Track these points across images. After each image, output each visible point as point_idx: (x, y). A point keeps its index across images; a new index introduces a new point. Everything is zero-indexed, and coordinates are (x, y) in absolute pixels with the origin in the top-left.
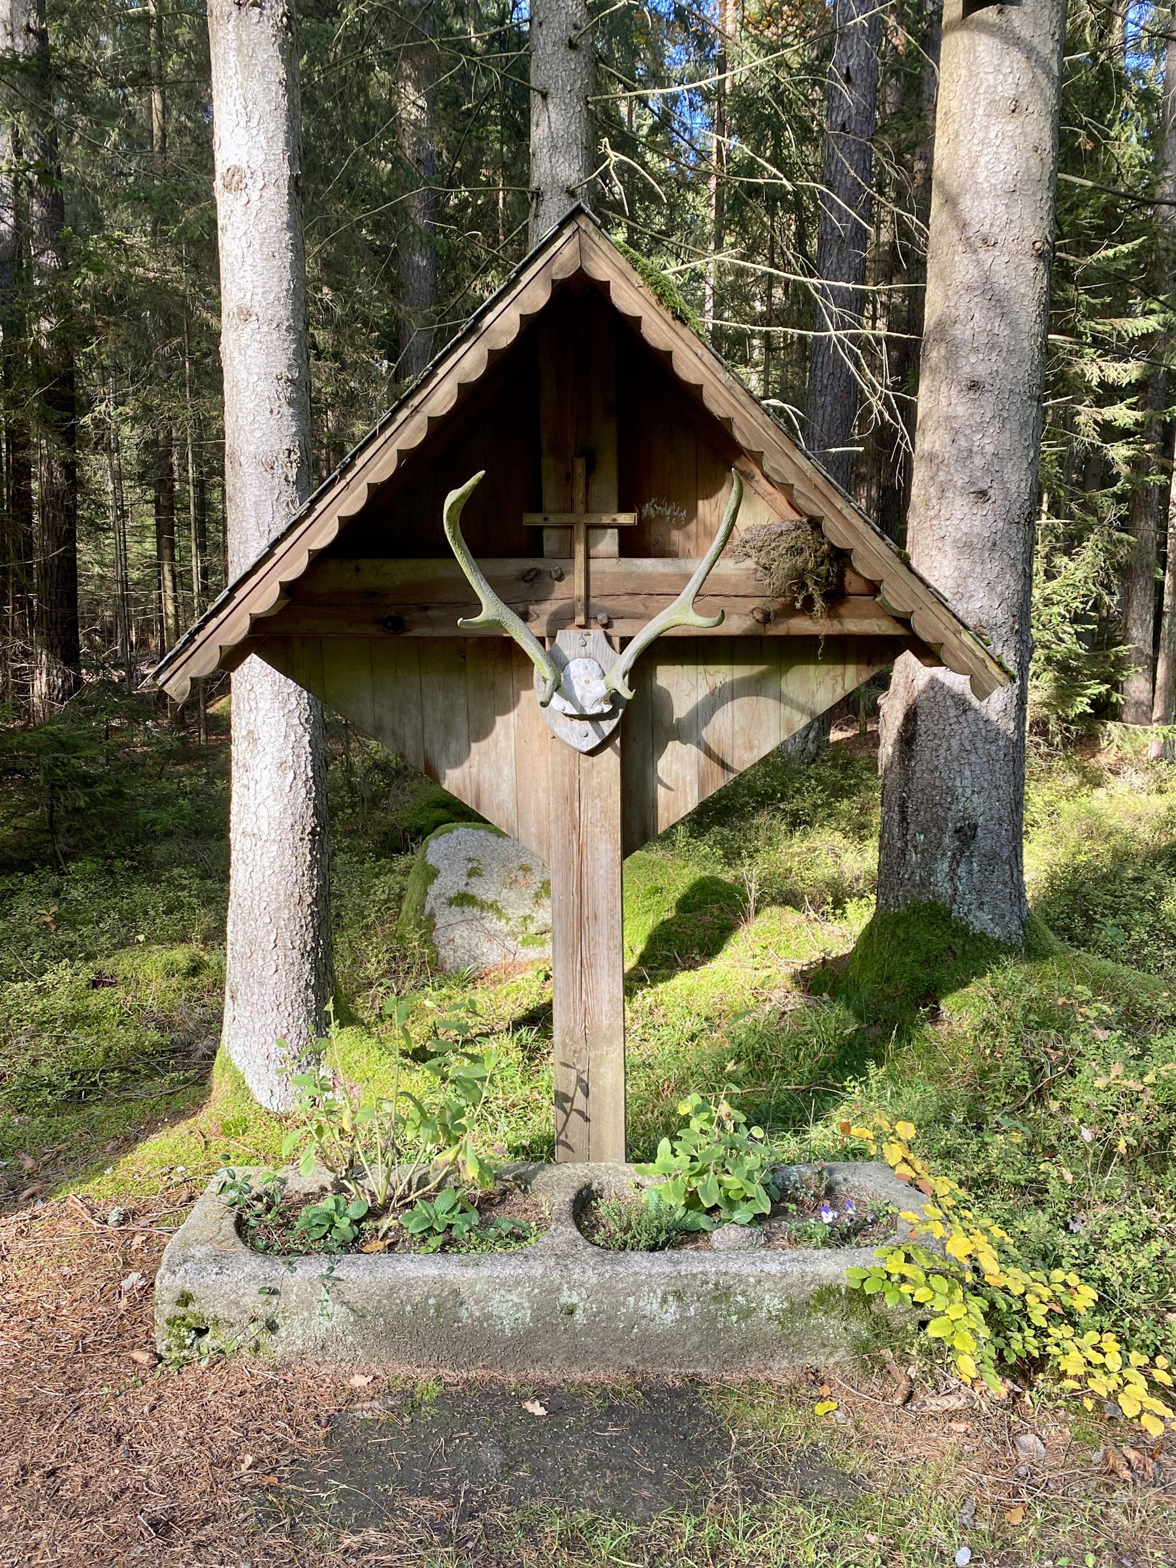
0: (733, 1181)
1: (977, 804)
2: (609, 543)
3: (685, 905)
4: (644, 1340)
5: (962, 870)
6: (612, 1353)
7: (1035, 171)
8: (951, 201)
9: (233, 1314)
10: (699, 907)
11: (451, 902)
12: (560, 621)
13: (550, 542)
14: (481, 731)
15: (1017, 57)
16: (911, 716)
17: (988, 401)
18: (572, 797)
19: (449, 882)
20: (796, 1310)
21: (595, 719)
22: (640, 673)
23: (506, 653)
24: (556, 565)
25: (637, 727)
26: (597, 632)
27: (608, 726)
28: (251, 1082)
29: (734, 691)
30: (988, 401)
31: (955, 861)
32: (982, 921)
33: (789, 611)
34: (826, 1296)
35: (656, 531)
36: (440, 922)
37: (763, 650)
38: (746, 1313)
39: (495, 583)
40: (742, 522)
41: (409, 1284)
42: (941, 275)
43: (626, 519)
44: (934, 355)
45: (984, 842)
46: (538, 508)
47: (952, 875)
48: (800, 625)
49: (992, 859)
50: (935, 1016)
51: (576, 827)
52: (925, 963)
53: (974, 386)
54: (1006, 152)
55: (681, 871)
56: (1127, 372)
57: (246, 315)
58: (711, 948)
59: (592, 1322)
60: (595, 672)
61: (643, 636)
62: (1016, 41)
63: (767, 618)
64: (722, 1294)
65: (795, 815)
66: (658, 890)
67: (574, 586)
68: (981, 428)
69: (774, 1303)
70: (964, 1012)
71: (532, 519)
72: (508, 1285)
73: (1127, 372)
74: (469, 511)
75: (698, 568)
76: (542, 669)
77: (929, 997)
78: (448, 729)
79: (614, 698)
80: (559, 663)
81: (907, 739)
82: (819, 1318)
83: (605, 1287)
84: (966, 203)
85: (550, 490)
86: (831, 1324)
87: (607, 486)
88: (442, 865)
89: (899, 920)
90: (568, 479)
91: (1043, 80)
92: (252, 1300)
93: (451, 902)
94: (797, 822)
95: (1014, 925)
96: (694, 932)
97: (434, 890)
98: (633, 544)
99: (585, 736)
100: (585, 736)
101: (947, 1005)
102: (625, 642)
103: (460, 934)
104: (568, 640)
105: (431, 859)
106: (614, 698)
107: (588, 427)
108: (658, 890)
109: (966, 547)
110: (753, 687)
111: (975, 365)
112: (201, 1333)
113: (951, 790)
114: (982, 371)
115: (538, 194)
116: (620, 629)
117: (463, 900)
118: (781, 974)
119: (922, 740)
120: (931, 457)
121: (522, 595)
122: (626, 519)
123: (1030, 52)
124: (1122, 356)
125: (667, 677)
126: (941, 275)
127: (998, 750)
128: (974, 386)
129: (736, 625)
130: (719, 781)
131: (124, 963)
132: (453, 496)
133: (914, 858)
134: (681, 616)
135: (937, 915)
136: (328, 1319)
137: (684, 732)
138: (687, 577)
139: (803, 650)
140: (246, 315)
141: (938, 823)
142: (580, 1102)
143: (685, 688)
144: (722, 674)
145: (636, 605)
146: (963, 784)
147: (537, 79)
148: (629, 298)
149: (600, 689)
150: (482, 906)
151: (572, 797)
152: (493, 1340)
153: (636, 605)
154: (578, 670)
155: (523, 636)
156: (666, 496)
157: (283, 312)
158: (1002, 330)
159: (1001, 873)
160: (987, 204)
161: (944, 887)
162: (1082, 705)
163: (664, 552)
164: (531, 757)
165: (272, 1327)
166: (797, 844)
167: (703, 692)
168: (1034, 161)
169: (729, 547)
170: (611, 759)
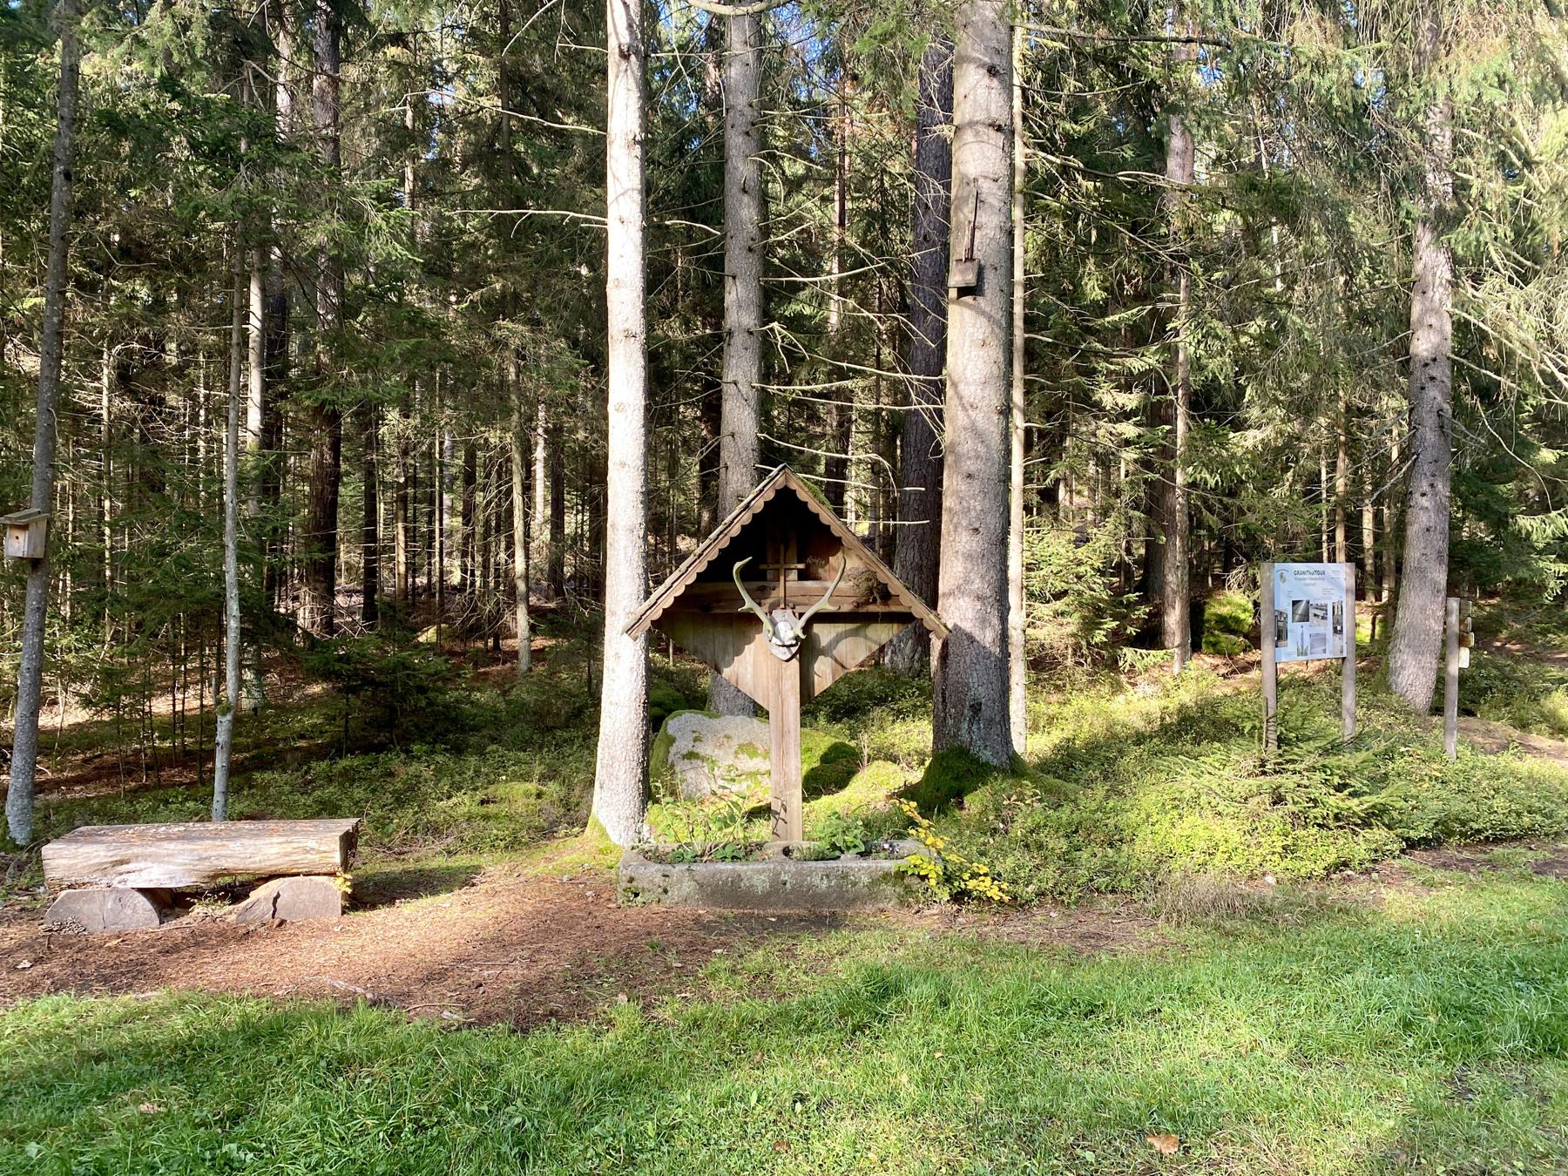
0: (849, 839)
1: (981, 690)
2: (793, 575)
3: (825, 759)
4: (814, 896)
5: (974, 728)
6: (801, 902)
7: (996, 372)
8: (955, 385)
9: (650, 886)
10: (834, 760)
11: (684, 757)
12: (774, 607)
13: (770, 575)
14: (739, 652)
15: (983, 321)
16: (945, 645)
17: (976, 484)
18: (779, 679)
19: (683, 745)
20: (874, 882)
21: (789, 647)
22: (807, 629)
23: (752, 620)
24: (772, 584)
25: (806, 650)
26: (789, 611)
27: (794, 650)
28: (609, 831)
29: (846, 635)
30: (976, 484)
31: (971, 723)
32: (986, 755)
33: (867, 603)
34: (886, 876)
35: (812, 570)
36: (677, 769)
37: (858, 618)
38: (854, 884)
39: (748, 591)
40: (848, 566)
41: (721, 872)
42: (952, 421)
43: (801, 566)
44: (949, 460)
45: (986, 712)
46: (765, 562)
47: (970, 730)
48: (872, 608)
49: (991, 721)
50: (961, 806)
51: (780, 692)
52: (956, 779)
53: (969, 476)
54: (980, 364)
55: (825, 738)
56: (1131, 400)
57: (623, 465)
58: (842, 784)
59: (793, 888)
60: (789, 627)
61: (809, 614)
62: (983, 313)
63: (858, 605)
64: (845, 876)
65: (900, 712)
66: (810, 750)
67: (779, 593)
68: (974, 497)
69: (866, 880)
70: (974, 802)
71: (763, 567)
72: (760, 872)
73: (1131, 400)
74: (742, 571)
75: (831, 586)
76: (767, 625)
77: (959, 795)
78: (725, 651)
79: (797, 638)
80: (774, 624)
81: (944, 657)
82: (883, 886)
83: (799, 873)
84: (961, 387)
85: (770, 555)
86: (888, 889)
87: (793, 553)
88: (678, 735)
89: (943, 757)
90: (777, 552)
91: (997, 330)
92: (658, 879)
93: (684, 757)
94: (900, 714)
95: (1004, 758)
96: (830, 774)
97: (673, 750)
98: (804, 576)
99: (785, 654)
100: (785, 654)
101: (967, 800)
102: (801, 615)
103: (690, 775)
104: (777, 614)
105: (670, 732)
106: (797, 638)
107: (790, 535)
108: (810, 750)
109: (969, 557)
110: (855, 633)
111: (971, 466)
112: (636, 895)
113: (967, 684)
114: (973, 469)
115: (730, 333)
116: (799, 609)
117: (691, 756)
118: (882, 794)
119: (951, 657)
120: (950, 510)
121: (759, 595)
122: (801, 566)
123: (990, 318)
124: (1127, 388)
125: (817, 628)
126: (952, 421)
127: (990, 663)
128: (969, 476)
129: (846, 608)
130: (841, 673)
131: (500, 790)
132: (738, 565)
133: (950, 722)
134: (824, 605)
135: (963, 752)
136: (688, 887)
137: (823, 652)
138: (826, 589)
139: (871, 618)
140: (623, 465)
141: (961, 702)
142: (783, 815)
143: (825, 633)
144: (841, 628)
145: (805, 600)
146: (973, 680)
147: (729, 267)
148: (803, 495)
149: (791, 634)
150: (703, 759)
151: (779, 679)
152: (755, 896)
153: (805, 600)
154: (781, 626)
155: (760, 612)
156: (816, 555)
157: (640, 463)
158: (981, 449)
159: (996, 730)
160: (972, 388)
161: (966, 738)
162: (1099, 637)
163: (816, 578)
164: (761, 664)
165: (666, 891)
166: (899, 727)
167: (833, 635)
168: (995, 368)
169: (841, 579)
170: (795, 663)
